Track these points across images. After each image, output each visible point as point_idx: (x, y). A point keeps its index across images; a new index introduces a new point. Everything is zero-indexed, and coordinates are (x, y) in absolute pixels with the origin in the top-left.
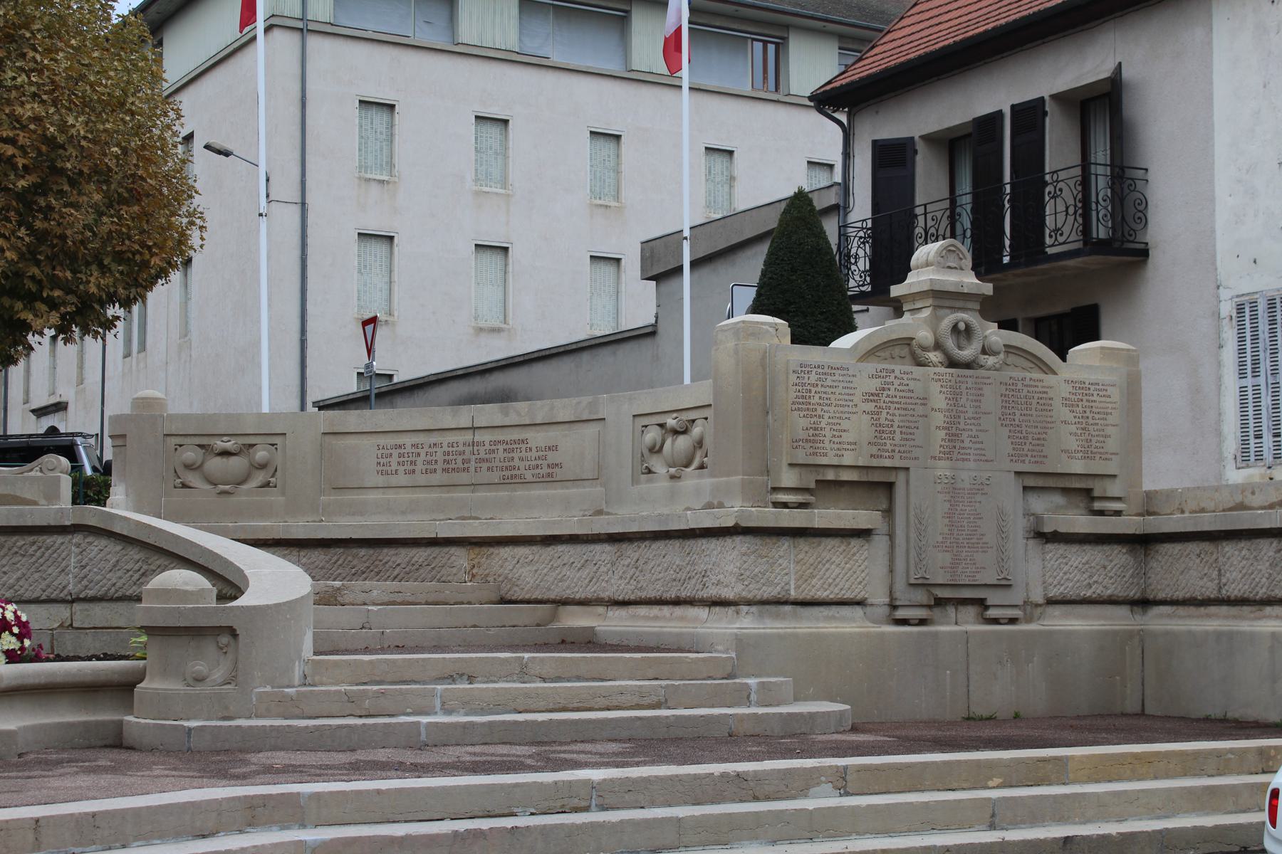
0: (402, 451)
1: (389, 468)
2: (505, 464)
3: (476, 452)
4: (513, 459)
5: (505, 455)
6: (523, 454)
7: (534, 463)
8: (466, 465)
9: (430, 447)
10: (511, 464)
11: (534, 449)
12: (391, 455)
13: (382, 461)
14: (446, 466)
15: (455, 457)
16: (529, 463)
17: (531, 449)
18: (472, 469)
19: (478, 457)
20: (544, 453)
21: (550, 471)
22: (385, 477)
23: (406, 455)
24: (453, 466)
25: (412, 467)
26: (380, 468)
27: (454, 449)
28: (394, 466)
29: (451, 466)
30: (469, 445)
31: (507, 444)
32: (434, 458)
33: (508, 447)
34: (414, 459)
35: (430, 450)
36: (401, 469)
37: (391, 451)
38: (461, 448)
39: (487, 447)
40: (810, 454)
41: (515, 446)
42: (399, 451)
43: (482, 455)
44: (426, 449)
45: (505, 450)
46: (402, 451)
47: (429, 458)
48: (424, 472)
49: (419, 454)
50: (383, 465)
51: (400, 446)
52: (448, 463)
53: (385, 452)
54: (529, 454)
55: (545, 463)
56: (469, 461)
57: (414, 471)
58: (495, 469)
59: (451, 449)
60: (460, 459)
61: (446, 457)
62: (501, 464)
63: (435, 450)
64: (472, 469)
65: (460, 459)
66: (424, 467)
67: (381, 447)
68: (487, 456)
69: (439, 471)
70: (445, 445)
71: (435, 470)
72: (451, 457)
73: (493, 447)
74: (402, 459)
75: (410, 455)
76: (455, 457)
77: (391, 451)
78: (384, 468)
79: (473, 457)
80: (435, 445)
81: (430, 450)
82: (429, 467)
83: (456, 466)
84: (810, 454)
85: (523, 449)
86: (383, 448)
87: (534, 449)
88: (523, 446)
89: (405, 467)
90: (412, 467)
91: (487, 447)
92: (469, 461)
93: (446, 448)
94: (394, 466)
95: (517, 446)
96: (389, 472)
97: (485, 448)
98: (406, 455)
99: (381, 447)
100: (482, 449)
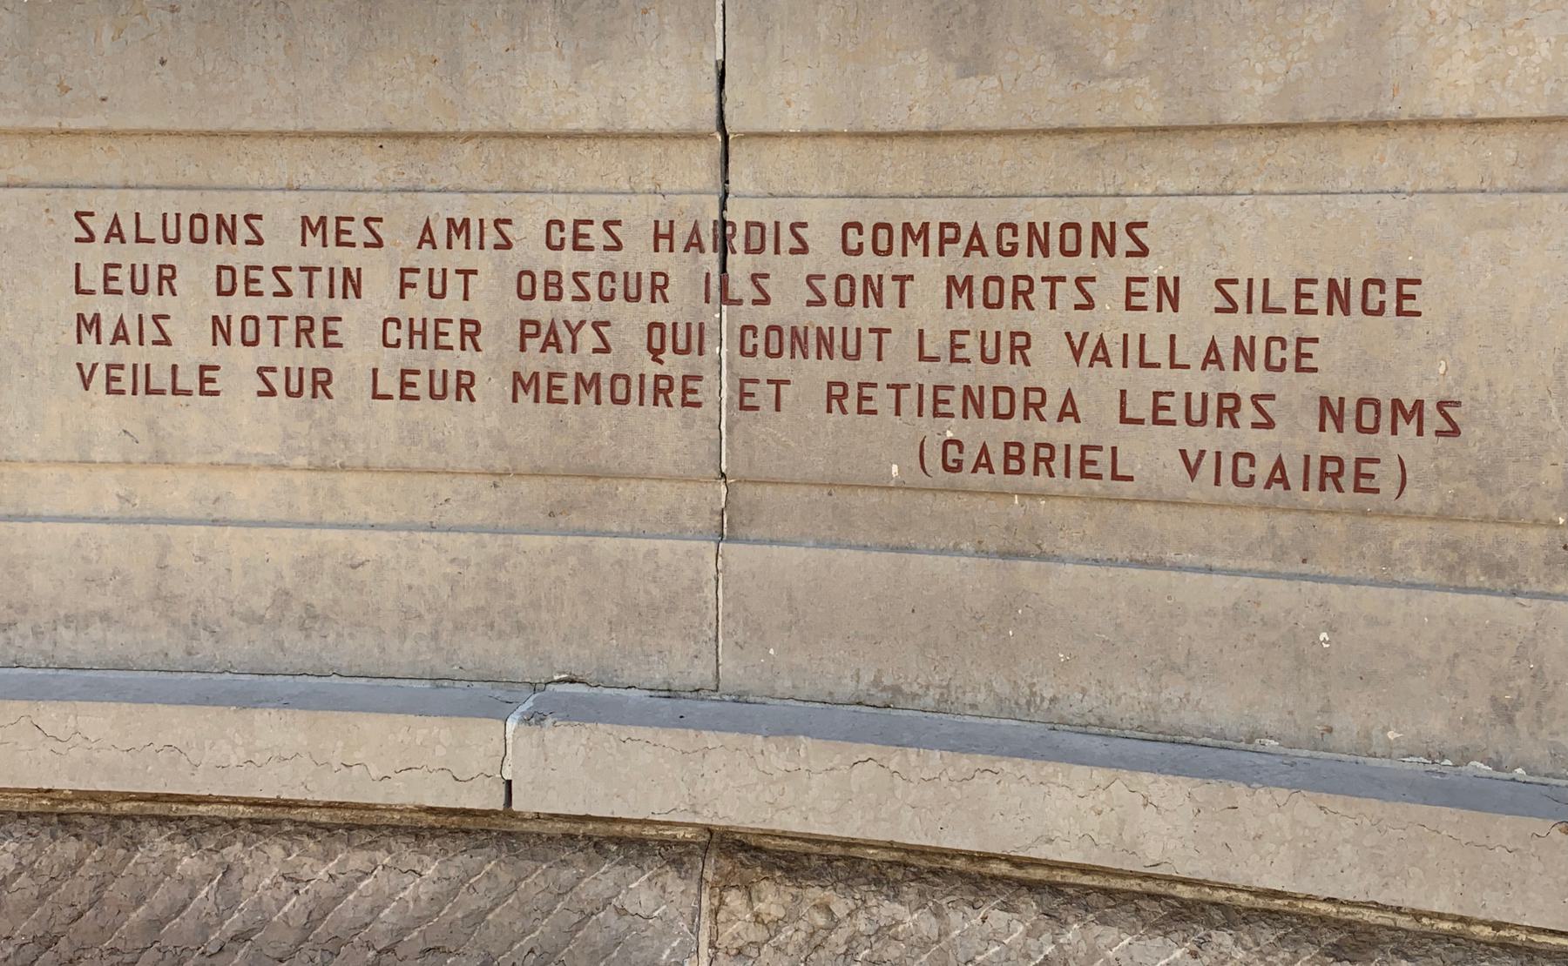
0: (240, 255)
1: (160, 359)
2: (960, 376)
3: (741, 286)
4: (1020, 345)
5: (961, 315)
6: (1109, 319)
7: (1199, 382)
8: (674, 364)
9: (427, 237)
10: (1008, 373)
11: (1198, 297)
12: (167, 276)
13: (109, 310)
14: (536, 360)
15: (595, 309)
16: (1164, 378)
17: (1169, 294)
18: (718, 390)
19: (763, 317)
20: (1288, 325)
21: (1344, 444)
22: (464, 826)
23: (268, 283)
24: (582, 360)
25: (310, 357)
26: (97, 353)
27: (593, 262)
28: (191, 347)
29: (569, 364)
30: (694, 243)
31: (976, 244)
32: (453, 307)
33: (979, 267)
34: (320, 306)
35: (426, 258)
36: (238, 361)
37: (171, 254)
38: (639, 258)
39: (826, 257)
40: (983, 461)
41: (1037, 267)
42: (219, 253)
43: (789, 307)
44: (401, 247)
45: (956, 286)
46: (240, 255)
47: (418, 305)
48: (389, 384)
49: (352, 282)
50: (120, 335)
51: (226, 228)
52: (552, 341)
53: (129, 254)
54: (1156, 325)
55: (1294, 392)
56: (694, 340)
57: (322, 381)
58: (882, 399)
59: (568, 261)
60: (630, 321)
61: (541, 309)
62: (930, 375)
63: (459, 257)
64: (718, 390)
65: (630, 321)
66: (390, 363)
67: (100, 227)
68: (825, 317)
69: (492, 386)
70: (528, 231)
71: (465, 385)
72: (570, 309)
73: (867, 264)
74: (240, 305)
75: (295, 280)
76: (595, 309)
77: (171, 254)
78: (128, 354)
79: (726, 320)
80: (459, 228)
81: (426, 258)
82: (422, 359)
83: (605, 366)
84: (983, 461)
85: (1109, 295)
86: (115, 232)
87: (1198, 297)
88: (1110, 273)
89: (265, 352)
90: (310, 357)
91: (826, 257)
92: (694, 340)
93: (531, 251)
94: (191, 347)
95: (1056, 264)
96: (161, 379)
97: (808, 264)
98: (268, 283)
99: (100, 227)
100: (787, 274)
